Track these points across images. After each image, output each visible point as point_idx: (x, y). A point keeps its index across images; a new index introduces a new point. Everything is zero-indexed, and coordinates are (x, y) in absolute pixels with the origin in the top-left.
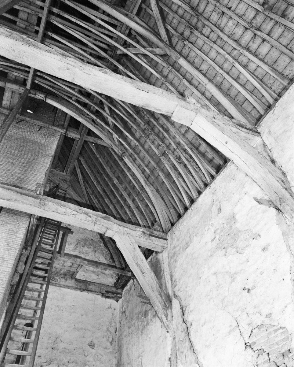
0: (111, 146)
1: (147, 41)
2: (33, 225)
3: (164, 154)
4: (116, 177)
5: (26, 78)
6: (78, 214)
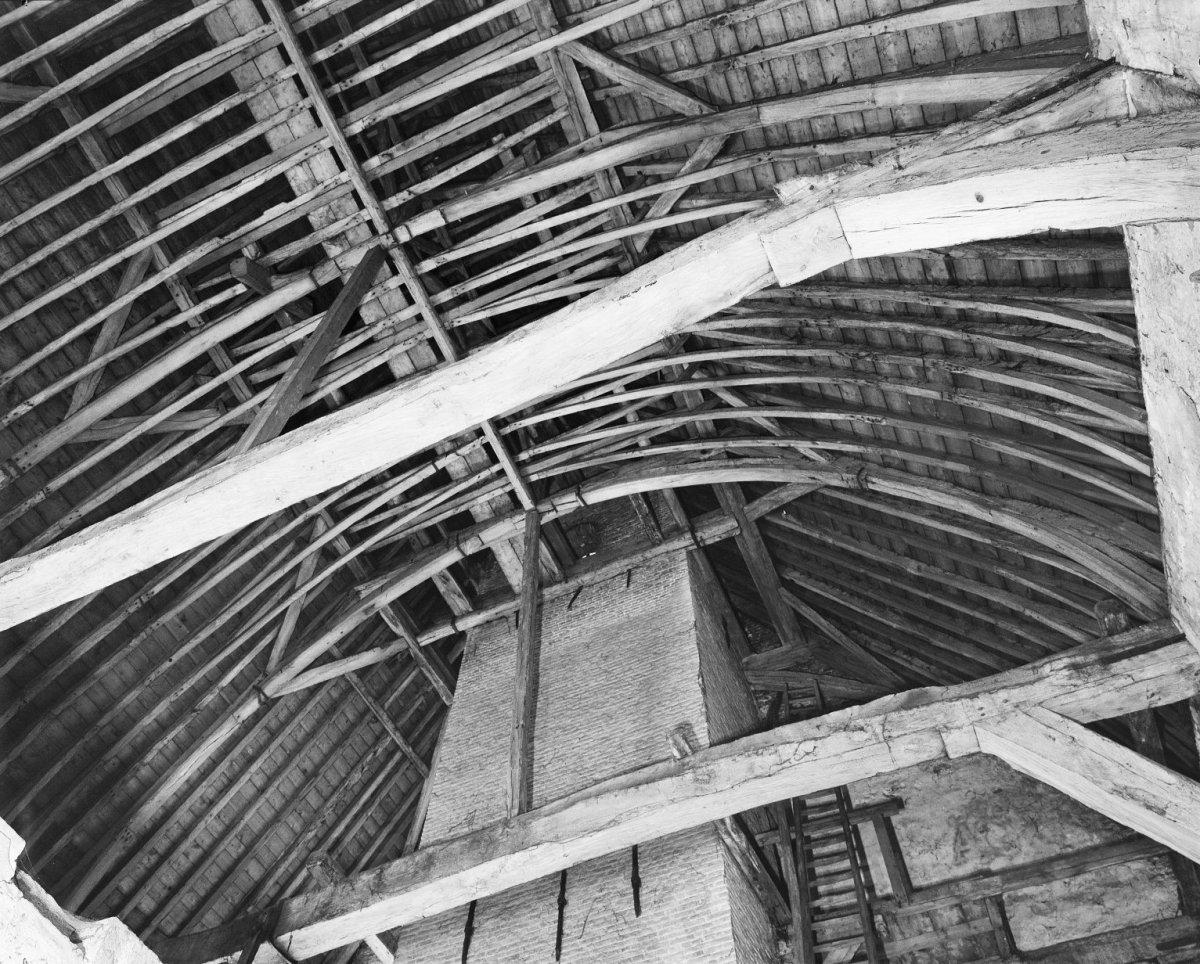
0: (813, 481)
1: (673, 155)
2: (743, 855)
3: (957, 383)
4: (906, 555)
5: (508, 489)
6: (819, 742)
